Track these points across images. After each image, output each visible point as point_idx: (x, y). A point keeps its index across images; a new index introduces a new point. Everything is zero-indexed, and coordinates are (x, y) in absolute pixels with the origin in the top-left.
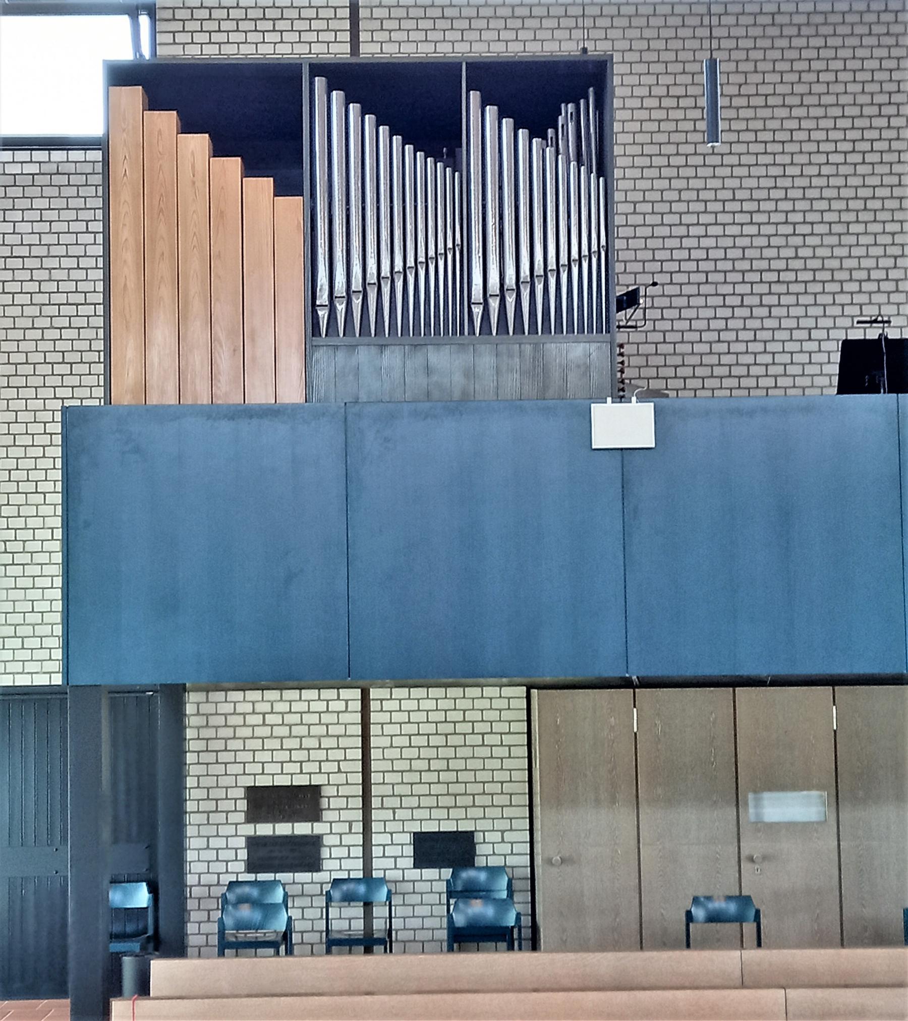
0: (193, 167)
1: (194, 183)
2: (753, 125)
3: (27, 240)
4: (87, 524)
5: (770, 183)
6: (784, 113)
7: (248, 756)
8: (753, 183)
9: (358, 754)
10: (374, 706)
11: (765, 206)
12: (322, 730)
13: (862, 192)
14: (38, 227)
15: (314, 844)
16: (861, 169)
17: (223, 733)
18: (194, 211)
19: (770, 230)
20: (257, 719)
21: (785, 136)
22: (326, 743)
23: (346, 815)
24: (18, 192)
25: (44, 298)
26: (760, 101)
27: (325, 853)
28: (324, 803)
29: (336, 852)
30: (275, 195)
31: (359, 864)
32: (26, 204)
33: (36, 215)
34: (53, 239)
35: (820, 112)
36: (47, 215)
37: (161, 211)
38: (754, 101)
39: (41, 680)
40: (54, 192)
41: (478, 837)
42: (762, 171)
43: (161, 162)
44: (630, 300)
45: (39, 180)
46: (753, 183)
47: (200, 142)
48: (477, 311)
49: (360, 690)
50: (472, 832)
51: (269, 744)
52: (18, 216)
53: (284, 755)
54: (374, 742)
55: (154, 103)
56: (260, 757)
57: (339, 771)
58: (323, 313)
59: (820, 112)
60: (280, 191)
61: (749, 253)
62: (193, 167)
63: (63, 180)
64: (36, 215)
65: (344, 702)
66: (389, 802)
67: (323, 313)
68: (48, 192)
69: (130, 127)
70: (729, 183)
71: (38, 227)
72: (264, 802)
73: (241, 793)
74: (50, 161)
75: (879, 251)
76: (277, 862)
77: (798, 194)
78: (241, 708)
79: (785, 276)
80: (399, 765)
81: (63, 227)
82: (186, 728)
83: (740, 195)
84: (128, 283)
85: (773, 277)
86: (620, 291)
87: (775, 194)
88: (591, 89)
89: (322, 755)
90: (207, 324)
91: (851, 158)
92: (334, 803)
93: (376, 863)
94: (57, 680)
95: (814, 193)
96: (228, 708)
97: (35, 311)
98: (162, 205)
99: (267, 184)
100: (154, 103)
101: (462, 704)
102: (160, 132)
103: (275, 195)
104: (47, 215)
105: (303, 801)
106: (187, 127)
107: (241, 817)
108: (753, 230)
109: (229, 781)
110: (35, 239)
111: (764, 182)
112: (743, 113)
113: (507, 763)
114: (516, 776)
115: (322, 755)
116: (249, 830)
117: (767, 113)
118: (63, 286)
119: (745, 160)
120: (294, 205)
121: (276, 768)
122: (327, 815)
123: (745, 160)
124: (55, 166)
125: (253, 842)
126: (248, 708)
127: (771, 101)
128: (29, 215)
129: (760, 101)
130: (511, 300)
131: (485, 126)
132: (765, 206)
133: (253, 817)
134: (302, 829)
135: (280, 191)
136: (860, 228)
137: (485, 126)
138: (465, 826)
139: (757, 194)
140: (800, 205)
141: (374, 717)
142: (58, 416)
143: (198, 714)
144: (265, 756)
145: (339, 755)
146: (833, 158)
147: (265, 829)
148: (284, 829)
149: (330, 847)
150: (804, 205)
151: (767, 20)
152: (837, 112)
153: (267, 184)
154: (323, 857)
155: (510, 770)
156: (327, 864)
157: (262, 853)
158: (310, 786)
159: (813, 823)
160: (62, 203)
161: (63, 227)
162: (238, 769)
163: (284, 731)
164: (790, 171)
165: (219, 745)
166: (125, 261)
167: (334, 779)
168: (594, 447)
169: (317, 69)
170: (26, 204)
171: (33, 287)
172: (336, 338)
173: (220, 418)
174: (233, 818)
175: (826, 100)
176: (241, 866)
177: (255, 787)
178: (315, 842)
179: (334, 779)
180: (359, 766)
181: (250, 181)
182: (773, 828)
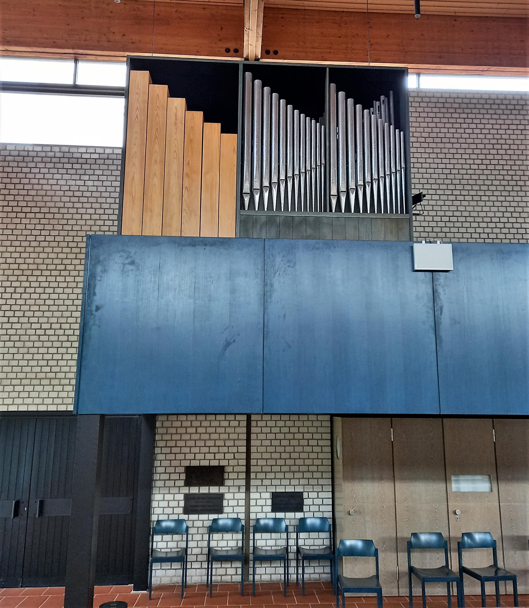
0: (176, 115)
1: (176, 124)
2: (436, 151)
3: (91, 189)
4: (98, 308)
5: (444, 176)
6: (450, 146)
7: (187, 450)
8: (436, 176)
9: (244, 449)
10: (253, 424)
11: (442, 187)
12: (226, 436)
13: (487, 182)
14: (96, 183)
15: (219, 498)
16: (486, 172)
17: (175, 437)
18: (176, 138)
19: (445, 198)
20: (193, 430)
21: (451, 156)
22: (228, 443)
23: (237, 482)
24: (88, 166)
25: (97, 217)
26: (439, 140)
27: (225, 503)
28: (226, 476)
29: (232, 503)
30: (222, 132)
31: (243, 509)
32: (91, 172)
33: (96, 178)
34: (103, 189)
35: (466, 146)
36: (101, 178)
37: (156, 138)
38: (436, 140)
39: (62, 408)
40: (105, 167)
41: (305, 495)
42: (440, 171)
43: (158, 111)
44: (418, 198)
45: (98, 161)
46: (436, 176)
47: (180, 103)
48: (334, 202)
49: (246, 416)
50: (303, 492)
51: (199, 443)
52: (87, 178)
53: (206, 450)
54: (253, 443)
55: (155, 80)
56: (194, 450)
57: (234, 458)
58: (247, 200)
59: (466, 146)
60: (224, 130)
61: (435, 208)
62: (176, 115)
63: (110, 162)
64: (96, 178)
65: (238, 422)
66: (260, 476)
67: (247, 200)
68: (102, 167)
69: (141, 92)
70: (425, 176)
71: (96, 183)
72: (196, 475)
73: (182, 470)
74: (104, 153)
75: (495, 209)
76: (199, 508)
77: (457, 182)
78: (184, 424)
79: (452, 219)
80: (265, 456)
81: (109, 183)
82: (155, 434)
83: (430, 181)
84: (135, 177)
85: (447, 219)
86: (415, 192)
87: (447, 182)
88: (391, 92)
89: (225, 449)
90: (180, 200)
91: (481, 167)
92: (232, 476)
93: (252, 509)
94: (71, 408)
95: (465, 182)
96: (178, 424)
97: (92, 223)
98: (157, 134)
99: (217, 126)
100: (155, 80)
101: (297, 424)
102: (158, 95)
103: (222, 132)
104: (101, 178)
105: (214, 475)
106: (172, 94)
107: (182, 483)
108: (437, 197)
109: (176, 463)
110: (94, 189)
111: (442, 176)
112: (431, 145)
113: (321, 456)
114: (325, 462)
115: (225, 449)
116: (186, 490)
117: (442, 145)
118: (107, 212)
119: (432, 166)
120: (232, 139)
121: (202, 456)
122: (228, 483)
123: (432, 166)
124: (107, 156)
125: (187, 497)
126: (189, 424)
127: (444, 140)
128: (92, 178)
129: (439, 140)
130: (352, 197)
131: (338, 101)
132: (442, 187)
133: (188, 483)
134: (214, 490)
135: (224, 130)
136: (486, 198)
137: (338, 101)
138: (299, 489)
139: (438, 181)
140: (458, 187)
141: (253, 430)
142: (85, 239)
143: (163, 427)
144: (196, 450)
145: (234, 450)
146: (473, 167)
147: (194, 490)
148: (204, 490)
149: (228, 500)
150: (461, 187)
151: (441, 105)
152: (474, 146)
153: (217, 126)
154: (224, 505)
155: (322, 459)
156: (226, 510)
157: (193, 503)
158: (219, 466)
159: (485, 492)
160: (109, 173)
161: (109, 183)
162: (182, 456)
163: (206, 437)
164: (453, 171)
165: (173, 444)
166: (134, 164)
167: (232, 463)
168: (416, 268)
169: (247, 68)
170: (91, 172)
171: (92, 211)
172: (254, 211)
173: (186, 245)
174: (178, 483)
175: (469, 141)
176: (181, 510)
177: (190, 466)
178: (221, 497)
179: (232, 463)
180: (244, 456)
181: (208, 125)
182: (464, 495)
